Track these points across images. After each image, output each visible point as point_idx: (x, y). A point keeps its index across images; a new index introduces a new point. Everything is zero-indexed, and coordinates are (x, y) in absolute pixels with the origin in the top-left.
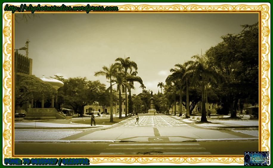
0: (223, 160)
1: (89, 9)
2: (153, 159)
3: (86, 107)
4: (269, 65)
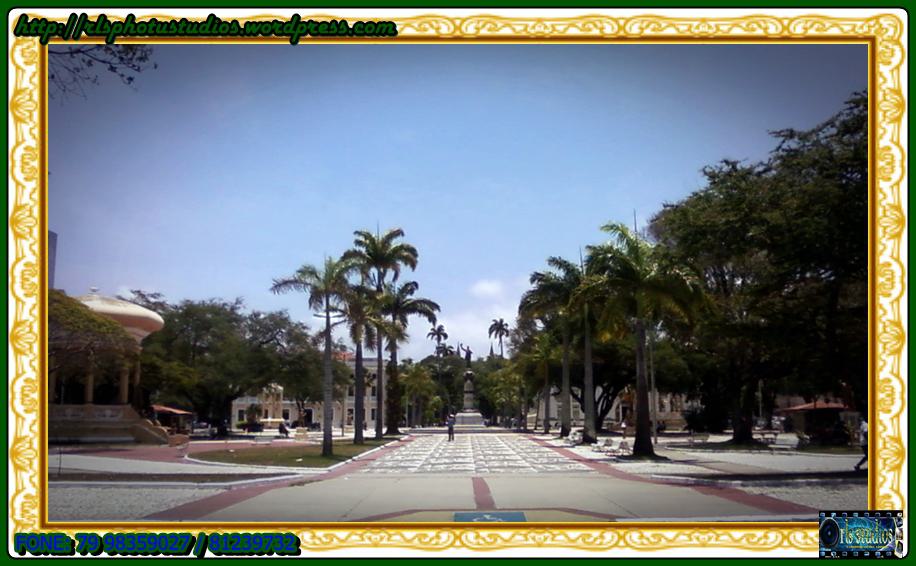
0: (748, 540)
1: (298, 31)
2: (513, 536)
3: (239, 404)
4: (903, 220)
